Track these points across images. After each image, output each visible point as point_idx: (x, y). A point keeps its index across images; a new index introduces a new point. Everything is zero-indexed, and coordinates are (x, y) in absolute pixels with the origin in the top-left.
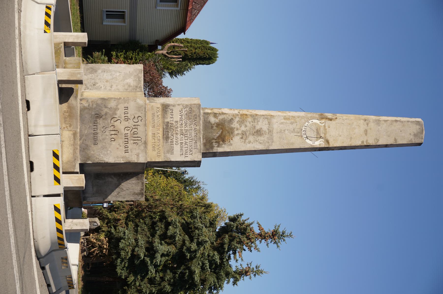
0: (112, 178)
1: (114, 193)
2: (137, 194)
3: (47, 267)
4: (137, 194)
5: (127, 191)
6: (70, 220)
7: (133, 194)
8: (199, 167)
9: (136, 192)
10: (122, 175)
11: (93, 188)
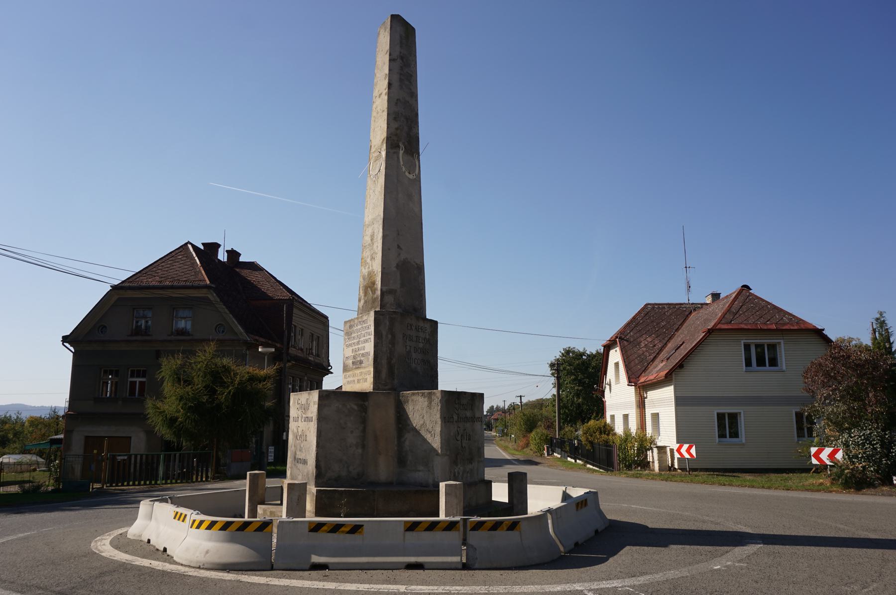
2: (430, 403)
3: (316, 559)
4: (430, 403)
7: (430, 408)
8: (393, 16)
9: (426, 403)
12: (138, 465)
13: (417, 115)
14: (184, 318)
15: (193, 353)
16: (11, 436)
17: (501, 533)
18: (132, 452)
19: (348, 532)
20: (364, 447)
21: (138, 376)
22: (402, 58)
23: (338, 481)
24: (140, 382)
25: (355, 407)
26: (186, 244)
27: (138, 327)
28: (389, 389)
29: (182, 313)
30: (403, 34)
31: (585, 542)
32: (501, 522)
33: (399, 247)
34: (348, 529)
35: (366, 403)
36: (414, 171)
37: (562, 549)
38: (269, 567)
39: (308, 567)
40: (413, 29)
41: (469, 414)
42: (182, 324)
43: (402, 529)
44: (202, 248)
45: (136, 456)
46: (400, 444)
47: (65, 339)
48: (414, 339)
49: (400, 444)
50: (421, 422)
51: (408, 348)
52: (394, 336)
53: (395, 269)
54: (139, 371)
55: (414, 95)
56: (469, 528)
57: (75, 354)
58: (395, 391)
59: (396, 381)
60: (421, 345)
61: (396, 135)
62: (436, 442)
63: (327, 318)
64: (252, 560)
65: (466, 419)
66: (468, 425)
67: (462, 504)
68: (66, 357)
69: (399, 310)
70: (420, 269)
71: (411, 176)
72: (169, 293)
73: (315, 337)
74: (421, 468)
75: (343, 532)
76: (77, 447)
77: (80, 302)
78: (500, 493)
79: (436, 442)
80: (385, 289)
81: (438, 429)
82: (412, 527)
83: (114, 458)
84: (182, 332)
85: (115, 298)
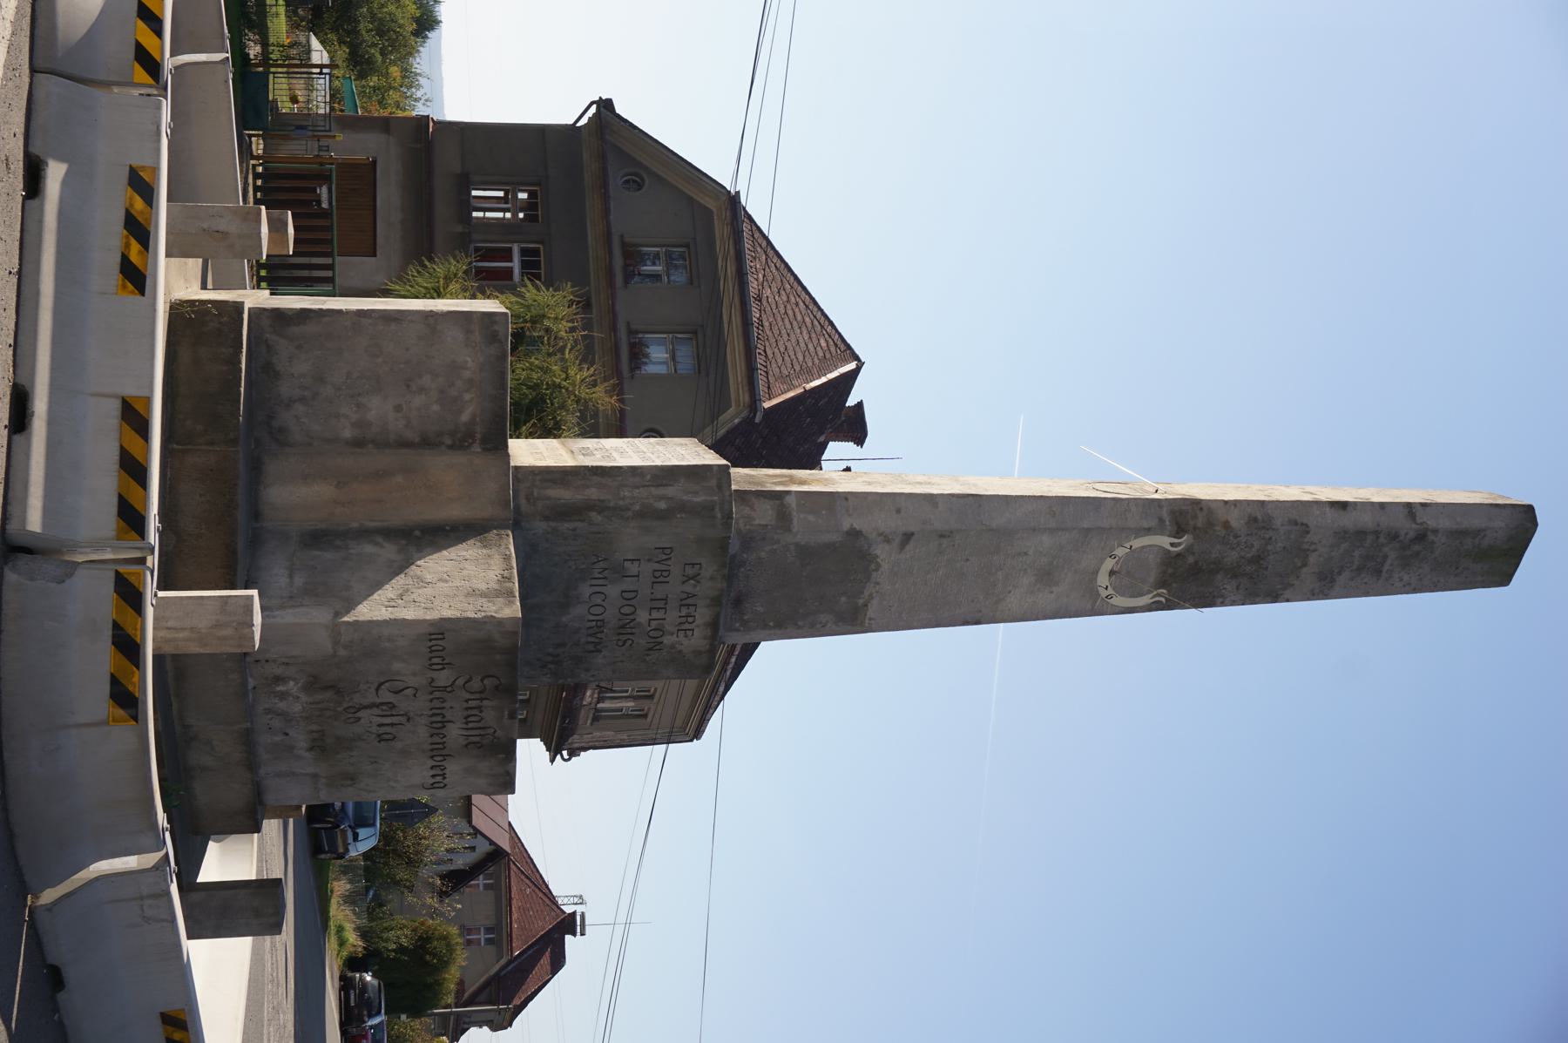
0: (376, 544)
1: (388, 591)
2: (483, 595)
3: (55, 173)
4: (483, 595)
5: (441, 584)
6: (274, 876)
7: (468, 595)
8: (1530, 510)
9: (483, 587)
10: (417, 533)
11: (291, 576)
12: (305, 273)
13: (1274, 597)
14: (673, 358)
15: (587, 358)
16: (373, 81)
17: (104, 656)
18: (338, 259)
19: (125, 259)
20: (358, 443)
21: (524, 265)
22: (1421, 537)
23: (264, 369)
24: (510, 270)
25: (465, 417)
26: (857, 358)
27: (641, 258)
28: (517, 509)
29: (686, 355)
30: (1484, 547)
31: (61, 1025)
32: (143, 429)
33: (908, 537)
34: (134, 257)
35: (477, 448)
36: (1121, 591)
37: (48, 896)
38: (39, 64)
39: (36, 149)
40: (1504, 578)
41: (455, 733)
42: (657, 356)
43: (130, 391)
44: (851, 401)
45: (331, 267)
46: (364, 534)
47: (605, 105)
48: (660, 591)
49: (364, 534)
50: (429, 578)
51: (633, 568)
52: (662, 516)
53: (846, 526)
54: (537, 265)
55: (1325, 586)
56: (122, 569)
57: (572, 128)
58: (516, 524)
59: (540, 526)
60: (643, 616)
61: (1210, 524)
62: (374, 609)
63: (697, 734)
64: (60, 35)
65: (439, 724)
66: (423, 732)
67: (195, 649)
68: (558, 105)
69: (735, 546)
70: (852, 620)
71: (1103, 579)
72: (729, 288)
73: (645, 704)
74: (299, 580)
75: (127, 245)
76: (346, 147)
77: (690, 124)
78: (225, 862)
79: (374, 609)
80: (790, 500)
81: (409, 614)
82: (134, 417)
83: (325, 178)
84: (637, 354)
85: (711, 204)
